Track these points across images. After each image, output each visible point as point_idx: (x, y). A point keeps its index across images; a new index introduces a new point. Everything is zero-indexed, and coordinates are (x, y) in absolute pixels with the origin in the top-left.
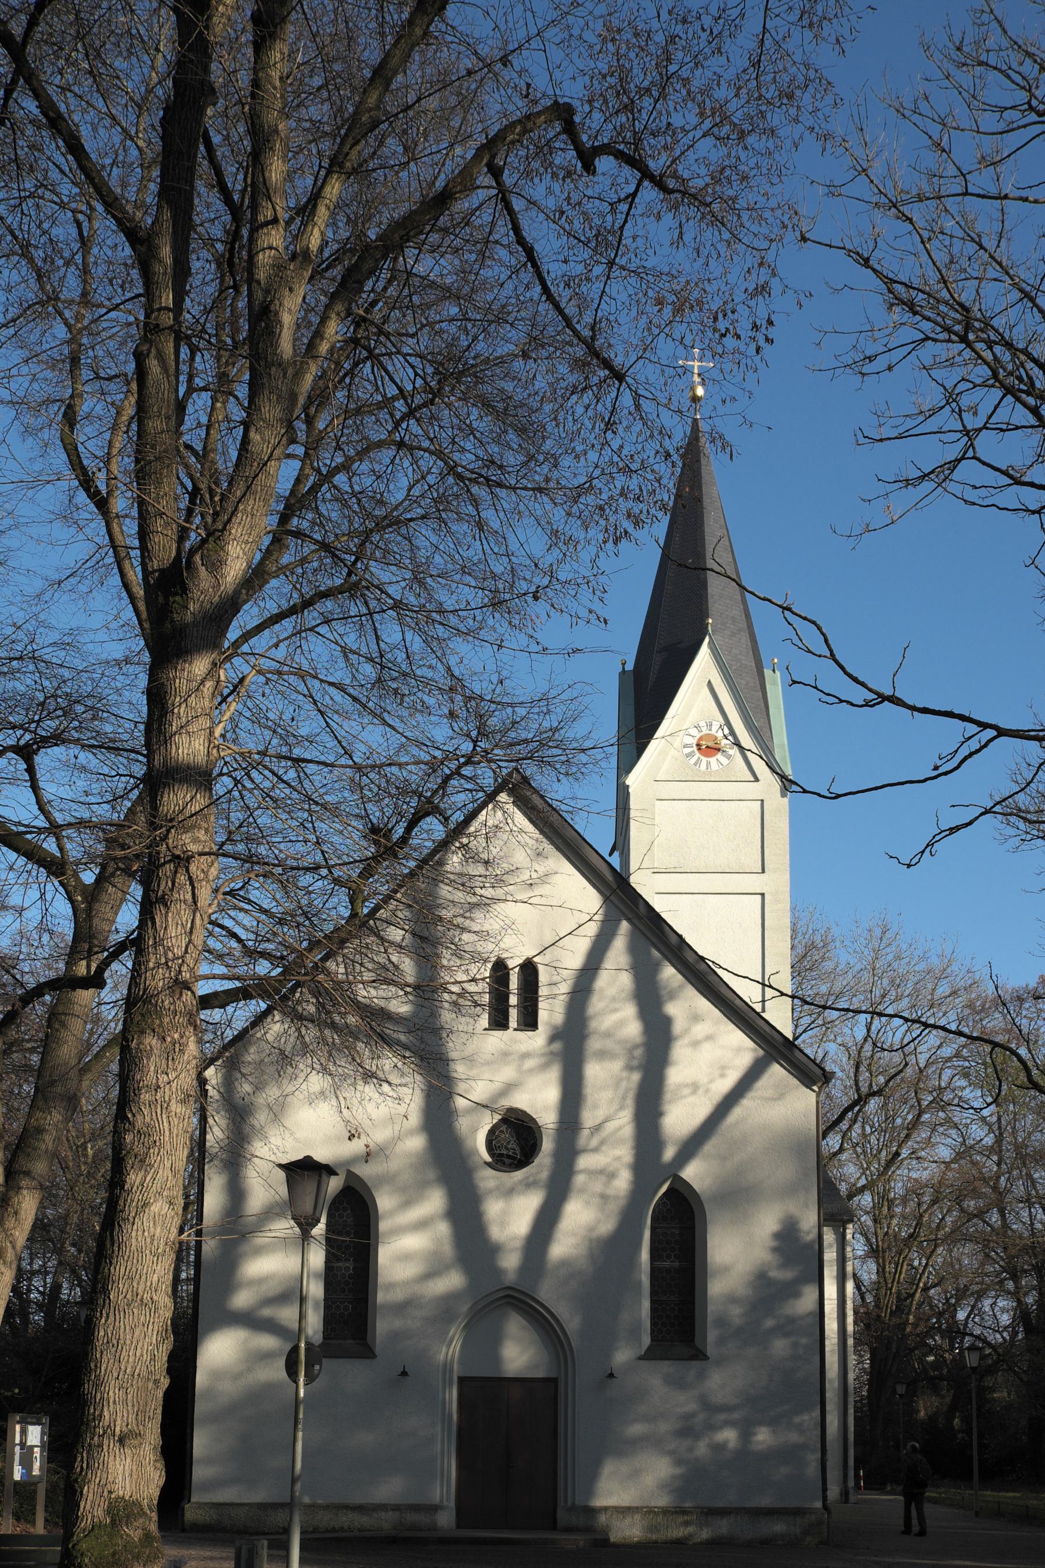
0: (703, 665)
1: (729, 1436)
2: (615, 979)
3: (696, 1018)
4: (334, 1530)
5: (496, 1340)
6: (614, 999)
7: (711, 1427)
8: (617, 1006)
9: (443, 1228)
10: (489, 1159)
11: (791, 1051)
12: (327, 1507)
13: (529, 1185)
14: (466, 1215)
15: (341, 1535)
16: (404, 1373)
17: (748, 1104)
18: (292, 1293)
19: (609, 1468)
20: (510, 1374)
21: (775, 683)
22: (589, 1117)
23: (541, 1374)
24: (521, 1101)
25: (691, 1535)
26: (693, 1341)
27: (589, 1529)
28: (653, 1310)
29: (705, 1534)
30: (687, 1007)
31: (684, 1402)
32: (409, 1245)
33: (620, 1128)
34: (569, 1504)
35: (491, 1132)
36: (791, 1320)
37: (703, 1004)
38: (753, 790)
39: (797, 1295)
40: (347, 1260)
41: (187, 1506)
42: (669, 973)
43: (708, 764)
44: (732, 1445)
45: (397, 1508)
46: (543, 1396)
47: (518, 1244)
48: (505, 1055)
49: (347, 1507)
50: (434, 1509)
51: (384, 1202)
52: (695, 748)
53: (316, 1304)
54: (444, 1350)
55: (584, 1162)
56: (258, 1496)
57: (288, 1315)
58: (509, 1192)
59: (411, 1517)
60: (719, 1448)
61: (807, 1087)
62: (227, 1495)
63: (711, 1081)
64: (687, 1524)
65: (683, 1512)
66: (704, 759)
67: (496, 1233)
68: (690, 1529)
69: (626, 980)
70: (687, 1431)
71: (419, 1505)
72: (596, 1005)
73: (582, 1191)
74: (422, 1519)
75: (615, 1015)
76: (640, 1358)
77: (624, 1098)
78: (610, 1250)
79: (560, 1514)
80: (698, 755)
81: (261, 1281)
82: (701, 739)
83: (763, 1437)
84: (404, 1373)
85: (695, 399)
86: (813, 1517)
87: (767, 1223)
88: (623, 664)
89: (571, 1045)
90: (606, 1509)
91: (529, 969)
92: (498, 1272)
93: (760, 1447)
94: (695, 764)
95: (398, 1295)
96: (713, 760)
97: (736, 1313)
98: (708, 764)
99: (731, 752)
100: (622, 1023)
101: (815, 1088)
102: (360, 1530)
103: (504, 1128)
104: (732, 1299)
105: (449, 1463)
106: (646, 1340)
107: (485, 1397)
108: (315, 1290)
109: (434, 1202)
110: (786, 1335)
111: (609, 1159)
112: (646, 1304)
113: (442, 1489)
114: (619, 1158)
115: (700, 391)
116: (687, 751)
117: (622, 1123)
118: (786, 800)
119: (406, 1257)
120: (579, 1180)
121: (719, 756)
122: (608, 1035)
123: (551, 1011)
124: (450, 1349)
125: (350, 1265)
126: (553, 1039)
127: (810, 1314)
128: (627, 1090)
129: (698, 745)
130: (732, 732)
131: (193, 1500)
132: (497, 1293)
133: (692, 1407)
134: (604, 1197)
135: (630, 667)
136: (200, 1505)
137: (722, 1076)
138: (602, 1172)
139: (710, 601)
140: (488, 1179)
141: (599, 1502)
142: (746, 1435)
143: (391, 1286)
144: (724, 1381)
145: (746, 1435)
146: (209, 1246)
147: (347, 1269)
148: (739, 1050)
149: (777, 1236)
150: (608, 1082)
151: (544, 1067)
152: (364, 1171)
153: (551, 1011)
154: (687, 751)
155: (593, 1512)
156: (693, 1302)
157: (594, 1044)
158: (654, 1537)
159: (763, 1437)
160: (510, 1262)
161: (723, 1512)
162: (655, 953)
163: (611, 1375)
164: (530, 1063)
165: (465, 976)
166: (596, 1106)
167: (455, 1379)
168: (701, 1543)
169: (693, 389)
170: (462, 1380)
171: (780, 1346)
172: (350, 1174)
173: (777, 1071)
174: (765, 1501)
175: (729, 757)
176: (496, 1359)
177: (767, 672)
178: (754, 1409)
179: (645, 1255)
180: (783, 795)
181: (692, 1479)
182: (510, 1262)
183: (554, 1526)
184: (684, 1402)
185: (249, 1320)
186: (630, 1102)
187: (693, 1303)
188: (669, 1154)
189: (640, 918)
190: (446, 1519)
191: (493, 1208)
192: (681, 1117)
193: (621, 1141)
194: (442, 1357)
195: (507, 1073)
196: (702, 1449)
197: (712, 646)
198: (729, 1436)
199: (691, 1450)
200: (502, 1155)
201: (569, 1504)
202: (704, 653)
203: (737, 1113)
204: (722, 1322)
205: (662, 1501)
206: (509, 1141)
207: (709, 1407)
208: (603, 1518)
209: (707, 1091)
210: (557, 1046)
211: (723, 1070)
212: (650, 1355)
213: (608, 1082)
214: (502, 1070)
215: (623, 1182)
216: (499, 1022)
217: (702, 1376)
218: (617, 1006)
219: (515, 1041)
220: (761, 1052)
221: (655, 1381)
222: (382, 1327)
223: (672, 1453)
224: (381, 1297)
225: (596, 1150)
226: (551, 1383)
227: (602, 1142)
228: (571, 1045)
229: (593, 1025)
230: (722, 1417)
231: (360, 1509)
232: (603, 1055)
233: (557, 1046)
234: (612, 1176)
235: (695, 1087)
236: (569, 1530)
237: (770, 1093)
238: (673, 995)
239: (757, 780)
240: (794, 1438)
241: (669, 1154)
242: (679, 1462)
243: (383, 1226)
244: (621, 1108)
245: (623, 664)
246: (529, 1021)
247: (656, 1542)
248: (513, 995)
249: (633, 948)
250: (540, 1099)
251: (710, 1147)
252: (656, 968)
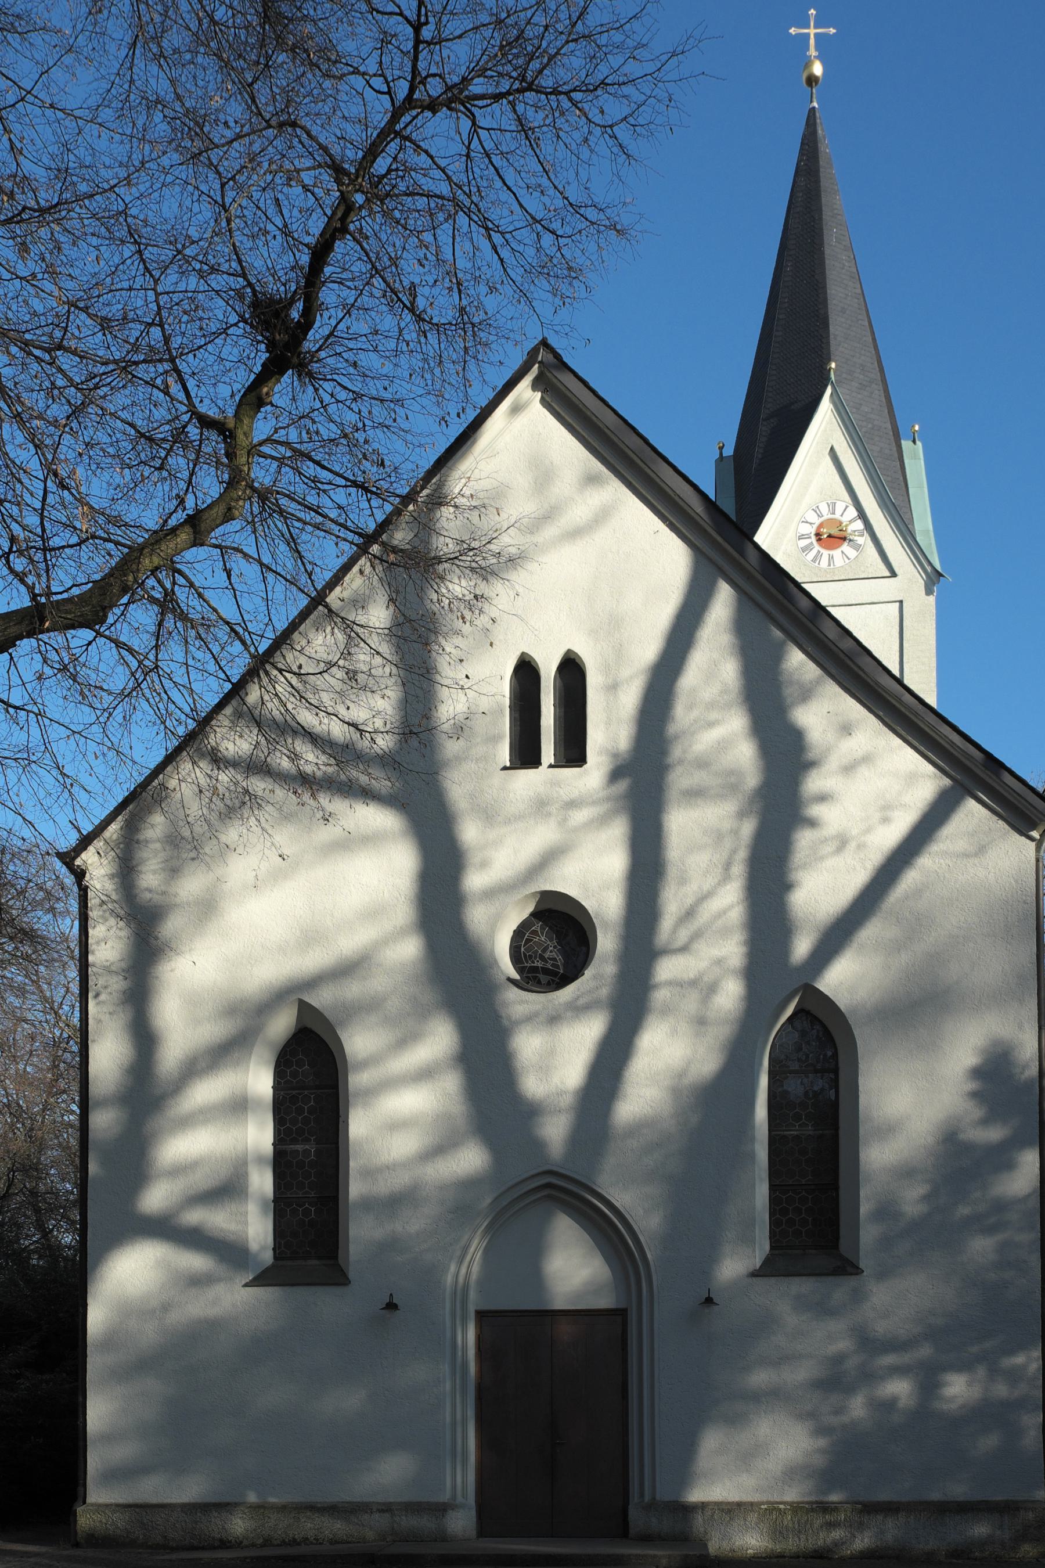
0: (824, 427)
1: (900, 1389)
2: (714, 666)
3: (846, 729)
4: (294, 1542)
5: (535, 1252)
6: (711, 706)
7: (869, 1377)
8: (713, 715)
9: (451, 1083)
10: (516, 976)
11: (998, 776)
12: (283, 1508)
13: (578, 1009)
14: (486, 1067)
15: (303, 1550)
16: (391, 1306)
17: (928, 863)
18: (227, 1189)
19: (712, 1442)
20: (559, 1304)
21: (915, 457)
22: (673, 901)
23: (605, 1302)
24: (568, 880)
25: (836, 1544)
26: (836, 1246)
27: (683, 1538)
28: (774, 1200)
29: (862, 1542)
30: (827, 714)
31: (831, 1338)
32: (402, 1111)
33: (723, 912)
34: (647, 1498)
35: (519, 934)
36: (1001, 1206)
37: (852, 708)
38: (889, 588)
39: (1010, 1166)
40: (307, 1140)
41: (79, 1510)
42: (797, 660)
43: (831, 558)
44: (902, 1403)
45: (386, 1508)
46: (608, 1336)
47: (567, 1101)
48: (540, 807)
49: (312, 1508)
50: (442, 1509)
51: (359, 1042)
52: (814, 539)
53: (264, 1204)
54: (453, 1268)
55: (667, 969)
56: (189, 1490)
57: (217, 1219)
58: (554, 1020)
59: (408, 1522)
60: (889, 1405)
61: (1021, 833)
62: (152, 1489)
63: (868, 830)
64: (831, 1525)
65: (824, 1508)
66: (826, 553)
67: (533, 1086)
68: (837, 1534)
69: (730, 671)
70: (834, 1381)
71: (419, 1504)
72: (683, 714)
73: (667, 1011)
74: (425, 1523)
75: (716, 731)
76: (754, 1274)
77: (728, 866)
78: (712, 1102)
79: (633, 1513)
80: (817, 547)
81: (178, 1170)
82: (821, 526)
83: (958, 1389)
84: (391, 1306)
85: (812, 80)
86: (1031, 1515)
87: (962, 1049)
88: (721, 448)
89: (644, 784)
90: (703, 1506)
91: (572, 669)
92: (538, 1146)
93: (953, 1406)
94: (814, 561)
95: (384, 1186)
96: (836, 553)
97: (912, 1199)
98: (831, 558)
99: (860, 540)
100: (723, 745)
101: (1035, 834)
102: (333, 1542)
103: (537, 926)
104: (906, 1172)
105: (465, 1437)
106: (762, 1247)
107: (521, 1343)
108: (262, 1182)
109: (439, 1040)
110: (991, 1230)
111: (707, 957)
112: (762, 1192)
113: (460, 1480)
114: (719, 962)
115: (818, 69)
116: (803, 543)
117: (729, 900)
118: (932, 599)
119: (396, 1125)
120: (660, 996)
121: (845, 547)
122: (702, 764)
123: (609, 727)
124: (467, 1266)
125: (312, 1147)
126: (616, 775)
127: (1029, 1196)
128: (734, 851)
129: (818, 535)
130: (862, 515)
131: (89, 1500)
132: (541, 1182)
133: (843, 1345)
134: (701, 1022)
135: (729, 451)
136: (100, 1508)
137: (886, 820)
138: (693, 983)
139: (833, 342)
140: (519, 1003)
141: (696, 1495)
142: (929, 1383)
143: (370, 1173)
144: (896, 1298)
145: (929, 1383)
146: (102, 1121)
147: (306, 1152)
148: (912, 778)
149: (977, 1073)
150: (706, 840)
151: (602, 821)
152: (322, 999)
153: (609, 727)
154: (803, 543)
155: (687, 1510)
156: (834, 1186)
157: (679, 779)
158: (779, 1548)
159: (958, 1389)
160: (555, 1131)
161: (889, 1508)
162: (777, 634)
163: (709, 1301)
164: (580, 816)
165: (475, 685)
166: (683, 881)
167: (472, 1315)
168: (852, 1557)
169: (808, 64)
170: (482, 1316)
171: (981, 1247)
172: (305, 1009)
173: (972, 814)
174: (958, 1490)
175: (857, 547)
176: (536, 1277)
177: (906, 444)
178: (949, 1341)
179: (761, 1112)
180: (929, 592)
181: (846, 1454)
182: (555, 1131)
183: (623, 1531)
184: (831, 1338)
185: (163, 1228)
186: (739, 869)
187: (836, 1188)
188: (802, 947)
189: (749, 577)
190: (462, 1523)
191: (528, 1045)
192: (821, 888)
193: (725, 932)
194: (449, 1279)
195: (540, 836)
196: (857, 1407)
197: (836, 400)
198: (900, 1389)
199: (839, 1411)
200: (535, 969)
201: (647, 1498)
202: (825, 408)
203: (910, 878)
204: (886, 1211)
205: (792, 1495)
206: (549, 948)
207: (869, 1344)
208: (699, 1521)
209: (861, 847)
210: (622, 786)
211: (886, 812)
212: (768, 1270)
213: (706, 840)
214: (540, 835)
215: (730, 994)
216: (526, 755)
217: (858, 1297)
218: (713, 715)
219: (555, 783)
220: (947, 782)
221: (783, 1298)
222: (361, 1233)
223: (811, 1415)
224: (356, 1189)
225: (684, 949)
226: (618, 1316)
227: (697, 936)
228: (644, 784)
229: (676, 752)
230: (889, 1360)
231: (333, 1510)
232: (695, 794)
233: (622, 786)
234: (712, 989)
235: (842, 842)
236: (646, 1538)
237: (961, 845)
238: (806, 694)
239: (894, 574)
240: (1001, 1390)
241: (802, 947)
242: (821, 1431)
243: (357, 1080)
244: (726, 877)
245: (721, 448)
246: (573, 751)
247: (781, 1556)
248: (547, 712)
249: (743, 629)
250: (595, 875)
251: (871, 932)
252: (778, 656)
